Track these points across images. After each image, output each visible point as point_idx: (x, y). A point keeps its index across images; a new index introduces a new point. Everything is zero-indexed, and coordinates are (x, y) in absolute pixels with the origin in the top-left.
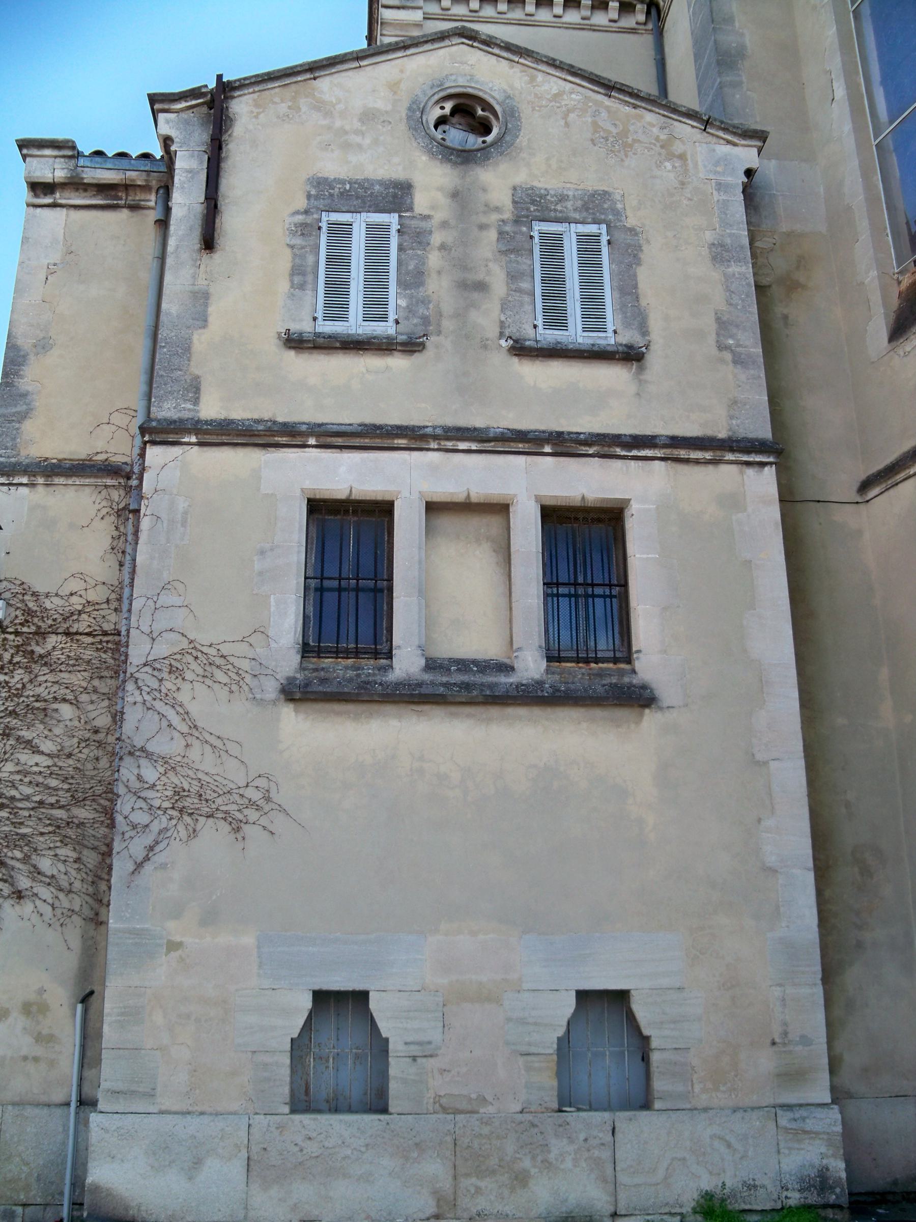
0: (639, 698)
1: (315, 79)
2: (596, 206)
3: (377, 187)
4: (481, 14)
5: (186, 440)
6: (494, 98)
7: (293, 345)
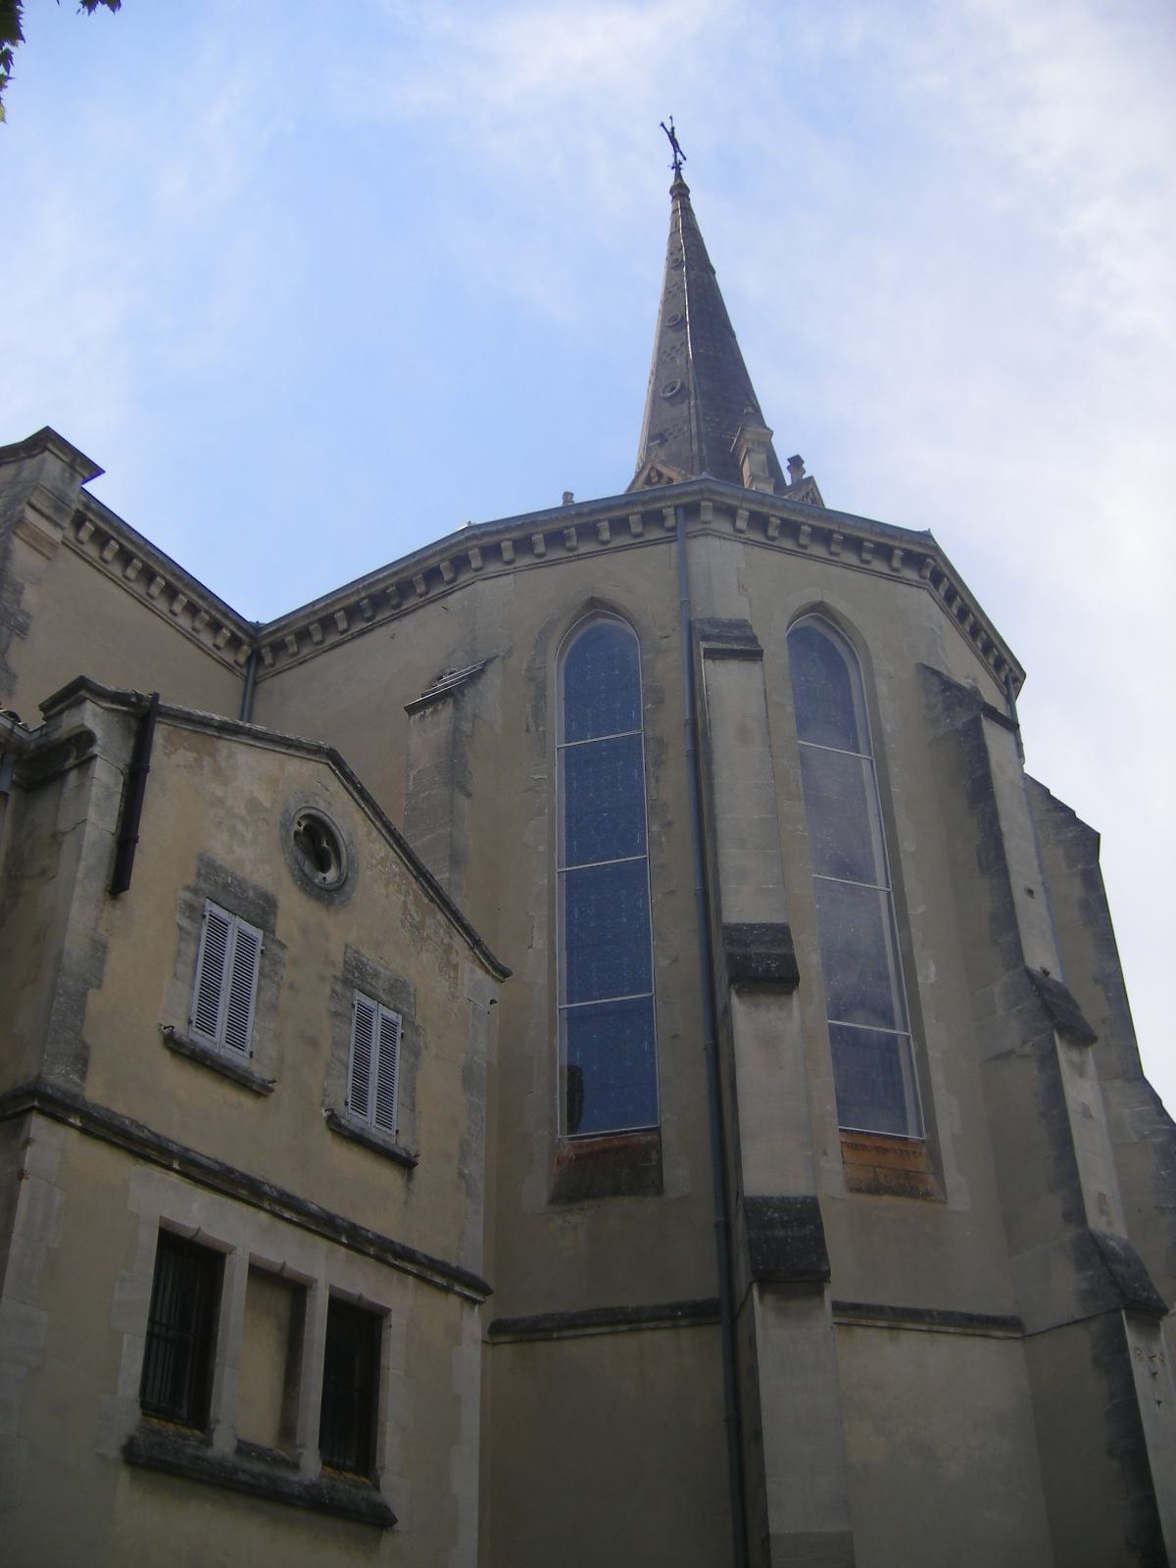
0: (380, 1520)
1: (218, 738)
4: (109, 567)
5: (72, 1120)
7: (171, 1045)
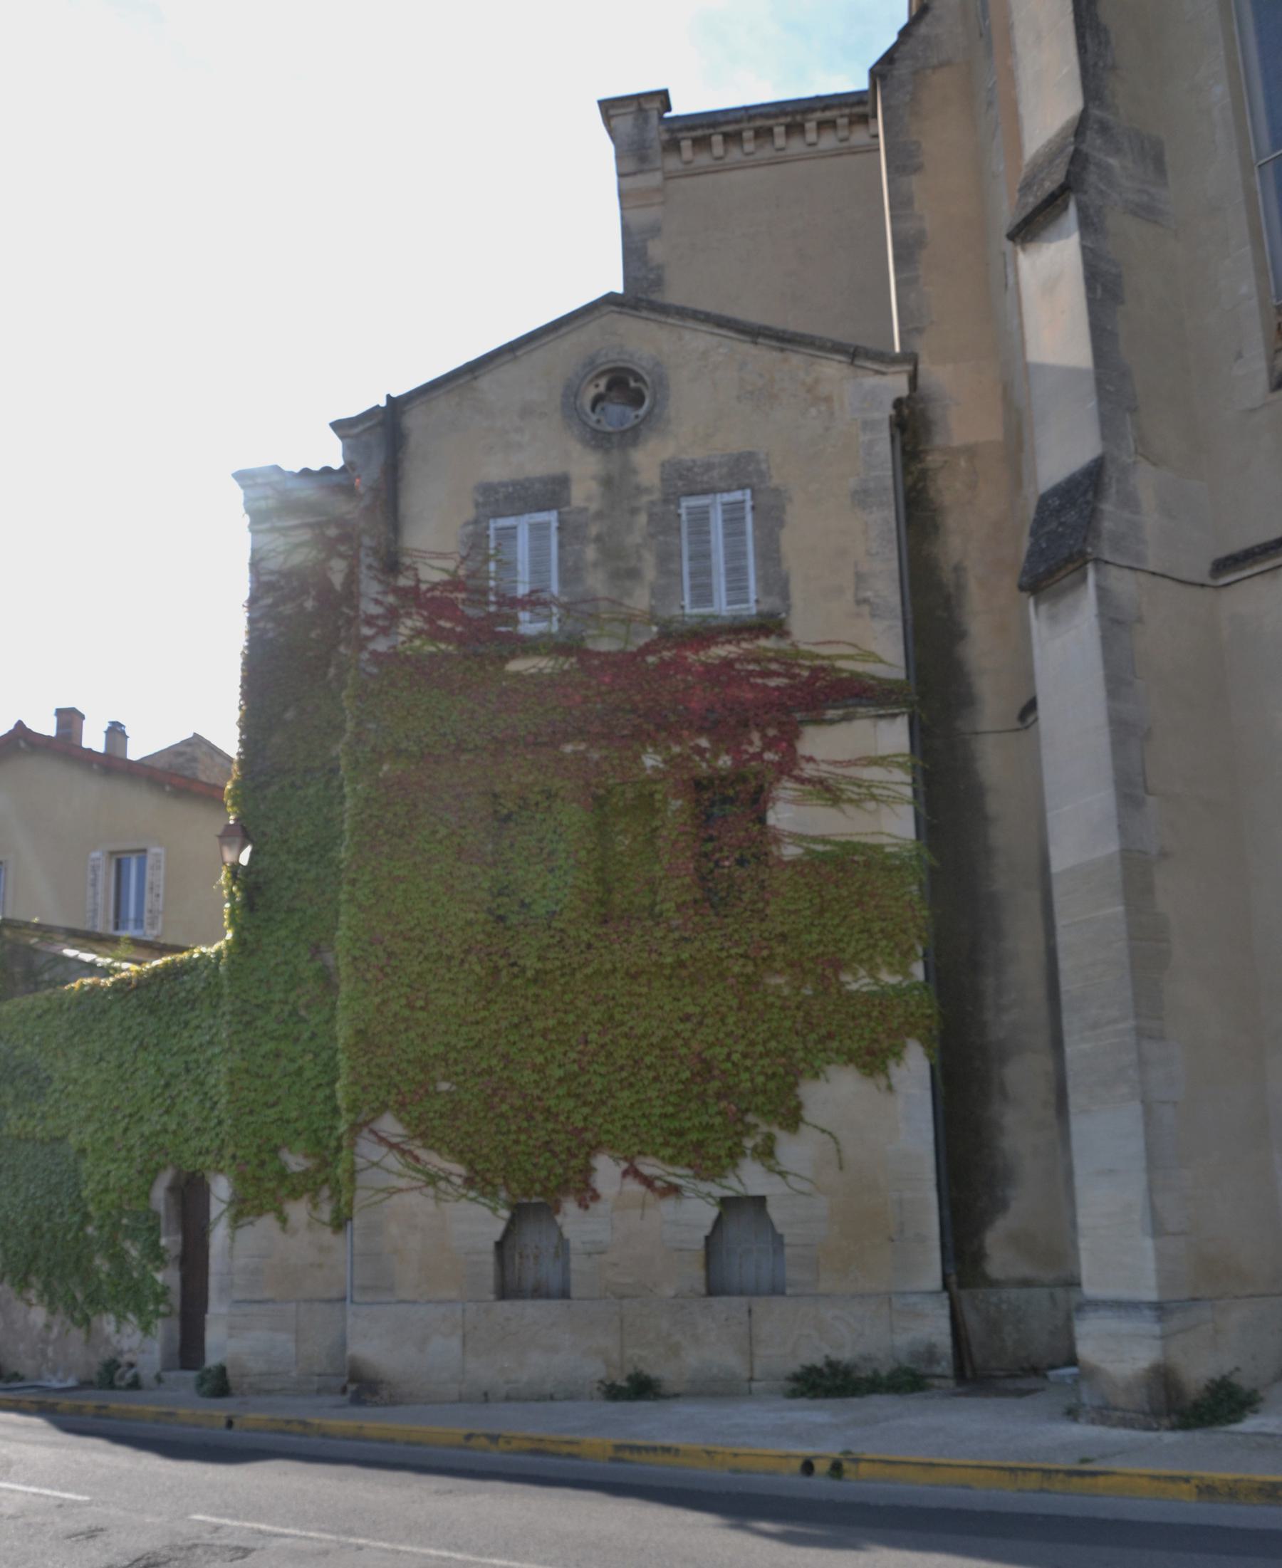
2: (742, 471)
3: (537, 486)
6: (643, 368)
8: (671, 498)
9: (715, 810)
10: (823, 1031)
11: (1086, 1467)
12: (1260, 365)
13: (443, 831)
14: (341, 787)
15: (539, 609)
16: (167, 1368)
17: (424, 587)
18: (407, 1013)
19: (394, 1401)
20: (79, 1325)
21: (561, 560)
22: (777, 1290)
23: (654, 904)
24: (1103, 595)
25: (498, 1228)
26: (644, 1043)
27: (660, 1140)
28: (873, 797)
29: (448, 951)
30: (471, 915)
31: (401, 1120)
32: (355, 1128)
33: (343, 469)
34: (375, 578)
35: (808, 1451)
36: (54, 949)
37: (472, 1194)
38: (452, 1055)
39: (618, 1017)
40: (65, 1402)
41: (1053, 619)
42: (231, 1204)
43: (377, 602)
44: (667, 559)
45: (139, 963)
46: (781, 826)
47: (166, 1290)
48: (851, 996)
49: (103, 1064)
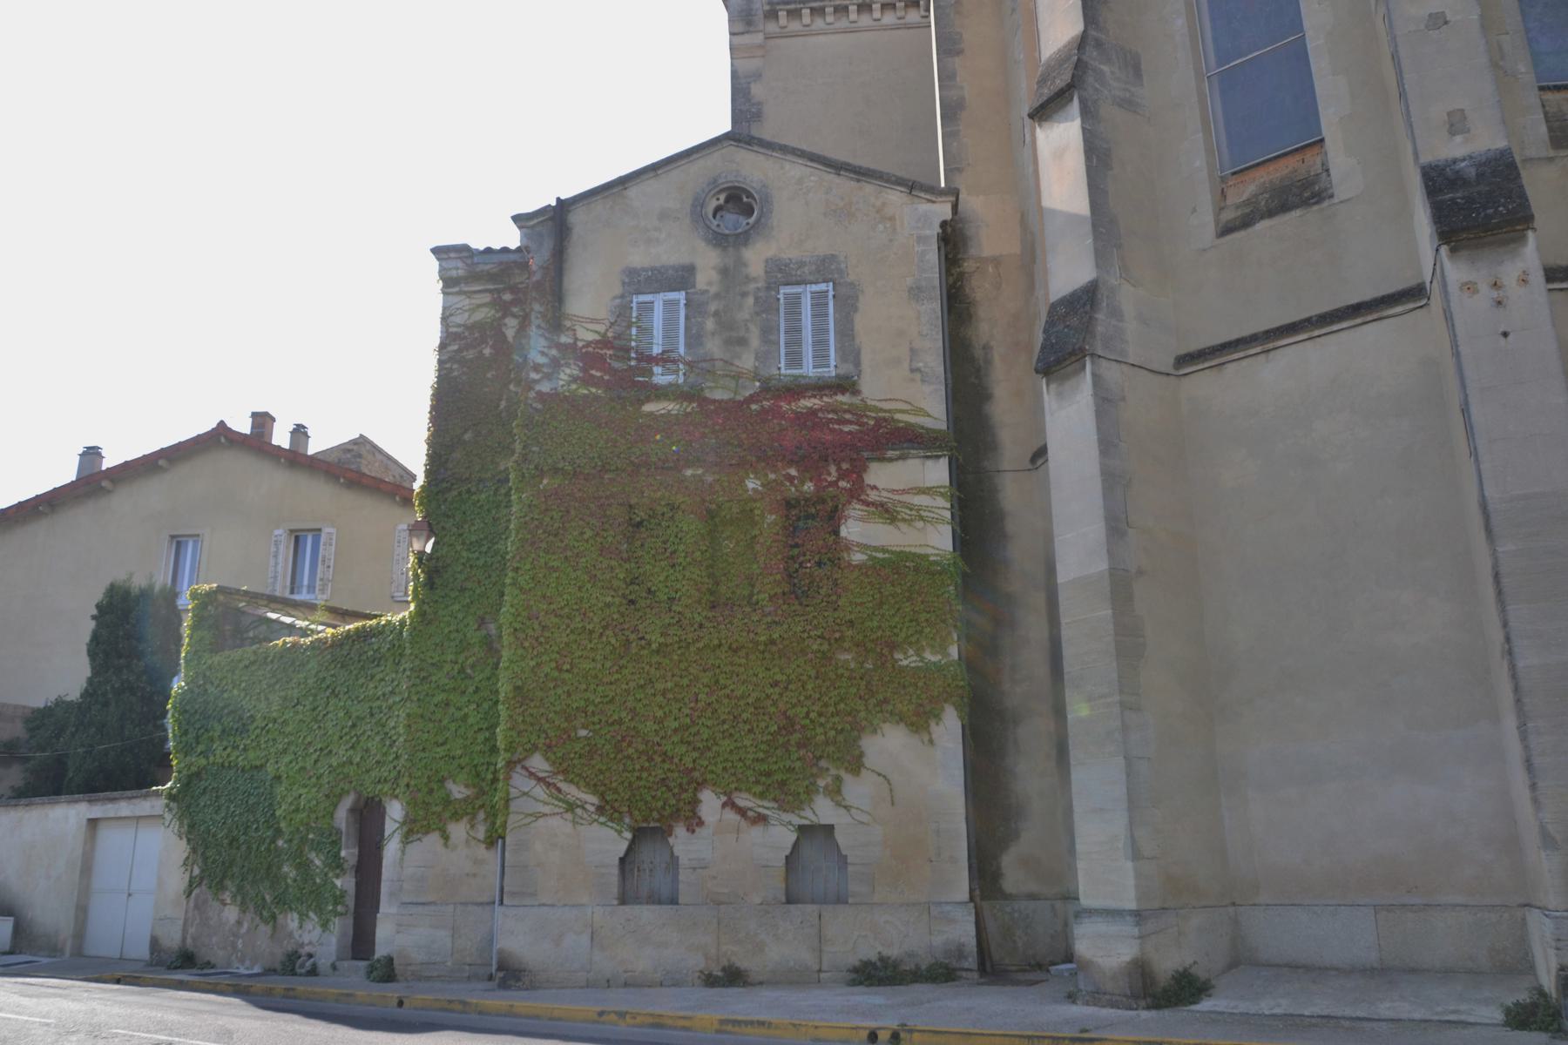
2: (826, 268)
8: (772, 286)
9: (801, 524)
10: (881, 697)
11: (1085, 1035)
12: (1209, 218)
13: (589, 533)
14: (508, 494)
15: (669, 365)
16: (340, 959)
17: (580, 344)
18: (556, 674)
19: (532, 987)
20: (266, 922)
21: (687, 329)
22: (841, 900)
23: (751, 596)
24: (1097, 379)
25: (624, 846)
26: (742, 703)
27: (752, 779)
28: (921, 518)
29: (590, 627)
30: (609, 599)
31: (547, 759)
32: (510, 765)
33: (519, 250)
34: (542, 335)
35: (873, 1024)
36: (260, 612)
37: (602, 819)
38: (591, 708)
39: (722, 682)
40: (258, 985)
41: (1060, 395)
42: (404, 823)
43: (543, 353)
44: (768, 332)
45: (334, 627)
46: (851, 538)
47: (343, 893)
48: (902, 669)
49: (300, 708)
